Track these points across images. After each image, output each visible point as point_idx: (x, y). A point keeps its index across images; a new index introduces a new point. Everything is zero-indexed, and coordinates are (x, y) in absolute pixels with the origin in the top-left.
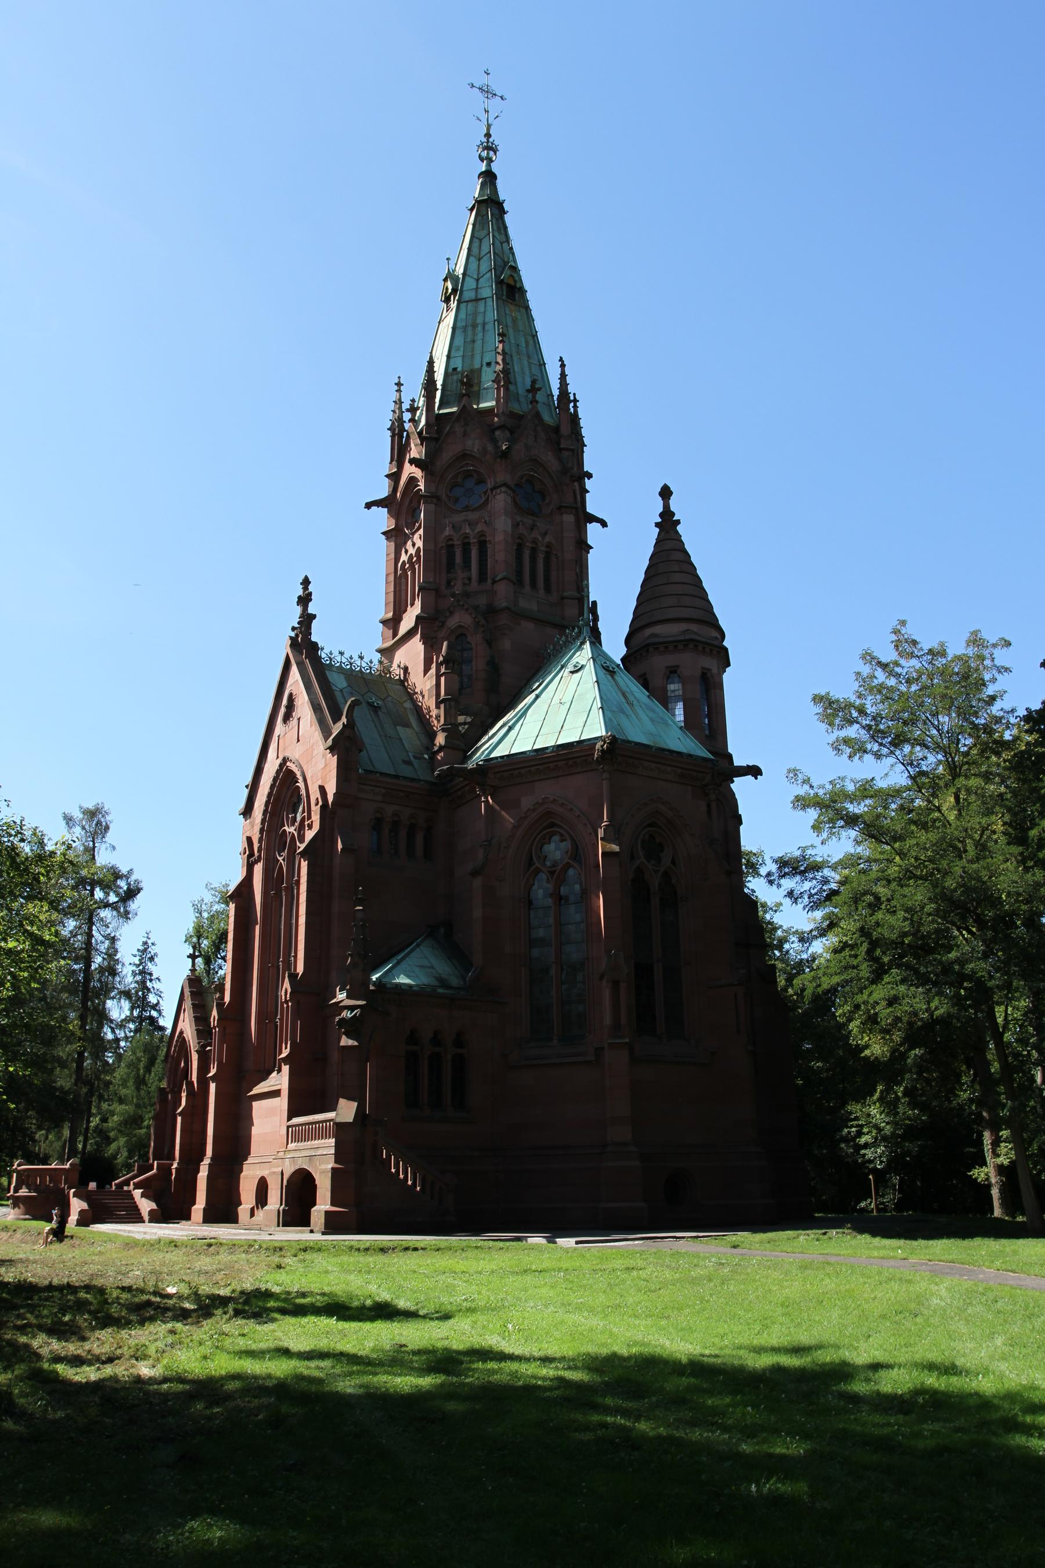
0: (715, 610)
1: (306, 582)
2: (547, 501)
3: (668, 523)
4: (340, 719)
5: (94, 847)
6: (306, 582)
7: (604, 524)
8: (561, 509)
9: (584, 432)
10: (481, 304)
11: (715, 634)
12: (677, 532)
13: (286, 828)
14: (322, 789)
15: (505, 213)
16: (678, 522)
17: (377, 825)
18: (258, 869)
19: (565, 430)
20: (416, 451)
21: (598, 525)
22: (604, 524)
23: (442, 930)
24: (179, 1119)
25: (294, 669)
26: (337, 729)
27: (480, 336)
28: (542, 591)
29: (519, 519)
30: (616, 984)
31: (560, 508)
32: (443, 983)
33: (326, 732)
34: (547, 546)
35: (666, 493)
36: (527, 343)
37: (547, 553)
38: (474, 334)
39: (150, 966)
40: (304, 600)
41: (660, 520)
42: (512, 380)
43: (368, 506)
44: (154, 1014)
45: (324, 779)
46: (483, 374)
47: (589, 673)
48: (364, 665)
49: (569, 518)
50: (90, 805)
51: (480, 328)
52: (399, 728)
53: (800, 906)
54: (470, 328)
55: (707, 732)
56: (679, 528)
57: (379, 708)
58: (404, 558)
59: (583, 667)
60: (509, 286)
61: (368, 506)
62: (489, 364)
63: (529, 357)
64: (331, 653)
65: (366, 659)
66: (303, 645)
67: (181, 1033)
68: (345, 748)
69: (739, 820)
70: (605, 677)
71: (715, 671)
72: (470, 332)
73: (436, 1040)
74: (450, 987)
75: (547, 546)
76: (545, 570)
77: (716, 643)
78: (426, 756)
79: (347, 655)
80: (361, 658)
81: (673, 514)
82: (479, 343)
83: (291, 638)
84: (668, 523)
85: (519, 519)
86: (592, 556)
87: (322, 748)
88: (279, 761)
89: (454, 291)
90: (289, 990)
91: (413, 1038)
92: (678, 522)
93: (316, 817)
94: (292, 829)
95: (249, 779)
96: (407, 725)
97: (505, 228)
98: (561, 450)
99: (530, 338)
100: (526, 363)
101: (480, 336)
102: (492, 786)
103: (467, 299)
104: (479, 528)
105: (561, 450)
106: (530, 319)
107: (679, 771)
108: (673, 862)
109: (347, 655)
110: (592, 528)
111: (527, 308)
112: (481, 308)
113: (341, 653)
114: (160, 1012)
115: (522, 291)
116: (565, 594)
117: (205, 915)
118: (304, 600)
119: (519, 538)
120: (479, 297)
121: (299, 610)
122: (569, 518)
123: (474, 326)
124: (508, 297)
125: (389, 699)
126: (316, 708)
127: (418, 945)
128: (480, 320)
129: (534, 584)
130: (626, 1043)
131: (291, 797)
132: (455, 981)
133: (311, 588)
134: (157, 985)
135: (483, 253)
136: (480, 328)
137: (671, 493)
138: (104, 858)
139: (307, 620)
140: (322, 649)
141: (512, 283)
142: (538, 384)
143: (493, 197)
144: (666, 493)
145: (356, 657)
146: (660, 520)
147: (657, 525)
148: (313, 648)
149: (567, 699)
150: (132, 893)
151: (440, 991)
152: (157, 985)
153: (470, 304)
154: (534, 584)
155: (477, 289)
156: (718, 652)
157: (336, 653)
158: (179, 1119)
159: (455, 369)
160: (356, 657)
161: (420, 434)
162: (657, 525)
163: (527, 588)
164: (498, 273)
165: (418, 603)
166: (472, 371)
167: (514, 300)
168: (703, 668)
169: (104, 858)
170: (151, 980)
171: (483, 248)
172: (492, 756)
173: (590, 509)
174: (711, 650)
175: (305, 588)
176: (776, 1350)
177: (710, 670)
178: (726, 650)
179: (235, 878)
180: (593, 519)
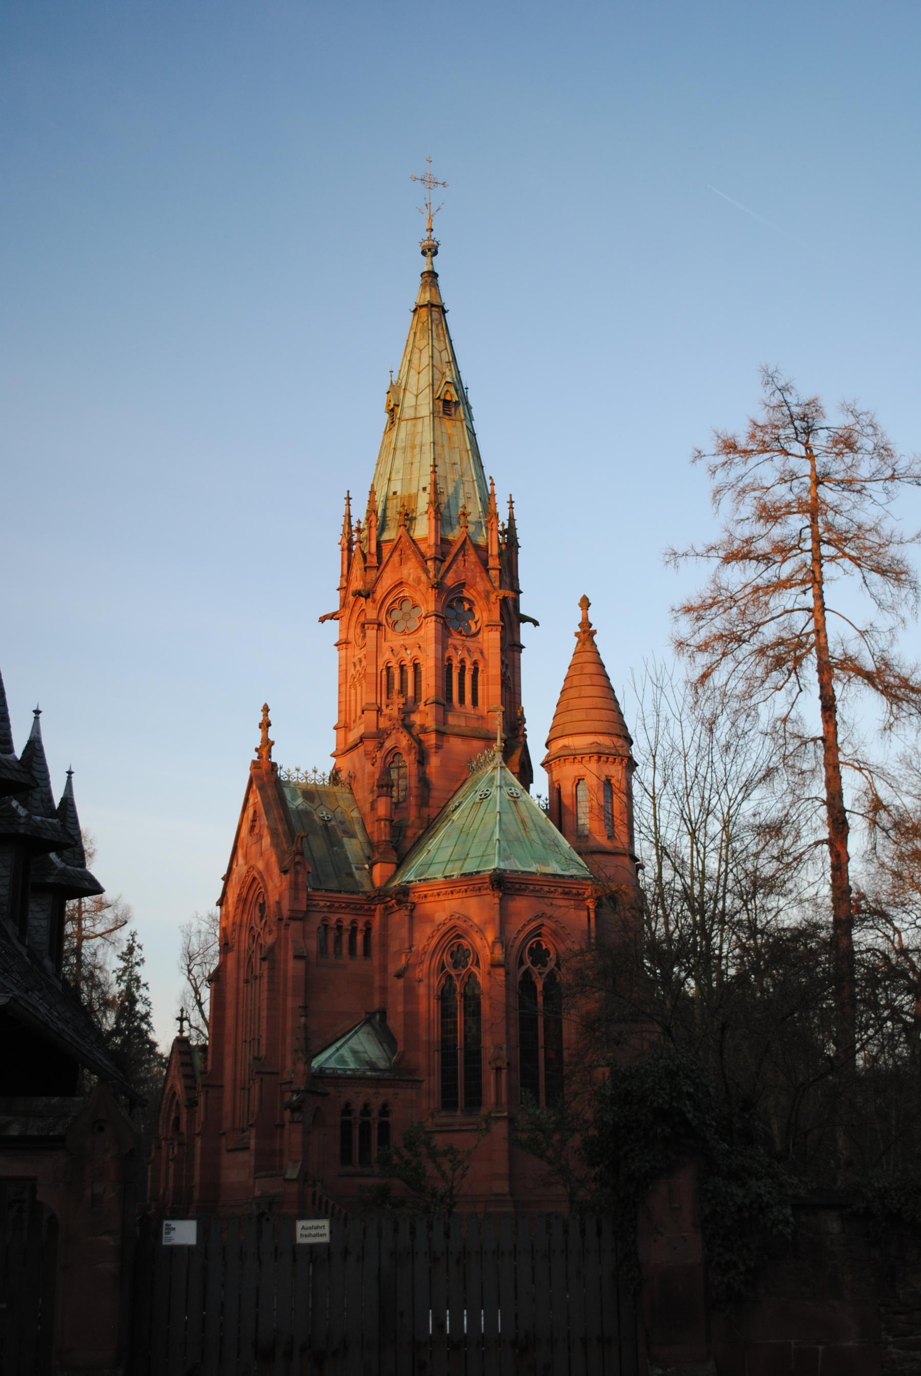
1: (266, 709)
3: (586, 633)
6: (266, 709)
7: (536, 623)
10: (420, 422)
16: (594, 632)
21: (531, 624)
22: (536, 623)
23: (378, 1017)
27: (418, 457)
30: (498, 1069)
32: (372, 1066)
35: (585, 603)
38: (413, 456)
39: (138, 971)
40: (266, 725)
41: (579, 630)
43: (322, 620)
44: (144, 1026)
46: (419, 500)
48: (318, 778)
51: (417, 450)
53: (389, 1119)
54: (409, 449)
61: (322, 620)
62: (424, 489)
64: (289, 771)
67: (172, 1087)
72: (409, 454)
73: (366, 1110)
74: (378, 1070)
79: (302, 771)
80: (315, 772)
82: (416, 465)
84: (586, 633)
86: (524, 656)
91: (347, 1110)
101: (418, 457)
103: (407, 417)
109: (302, 771)
110: (525, 628)
112: (419, 429)
113: (298, 770)
114: (149, 1024)
118: (266, 725)
120: (418, 416)
121: (259, 733)
123: (413, 447)
124: (445, 413)
127: (356, 1032)
128: (418, 442)
130: (505, 1117)
131: (257, 898)
132: (382, 1064)
135: (422, 366)
136: (417, 450)
137: (589, 604)
139: (267, 745)
144: (585, 603)
145: (310, 772)
146: (579, 630)
147: (577, 634)
151: (369, 1073)
152: (143, 991)
153: (410, 423)
155: (416, 406)
157: (293, 770)
159: (395, 493)
160: (310, 772)
162: (577, 634)
166: (410, 496)
168: (606, 776)
170: (138, 988)
171: (423, 360)
173: (523, 611)
175: (266, 715)
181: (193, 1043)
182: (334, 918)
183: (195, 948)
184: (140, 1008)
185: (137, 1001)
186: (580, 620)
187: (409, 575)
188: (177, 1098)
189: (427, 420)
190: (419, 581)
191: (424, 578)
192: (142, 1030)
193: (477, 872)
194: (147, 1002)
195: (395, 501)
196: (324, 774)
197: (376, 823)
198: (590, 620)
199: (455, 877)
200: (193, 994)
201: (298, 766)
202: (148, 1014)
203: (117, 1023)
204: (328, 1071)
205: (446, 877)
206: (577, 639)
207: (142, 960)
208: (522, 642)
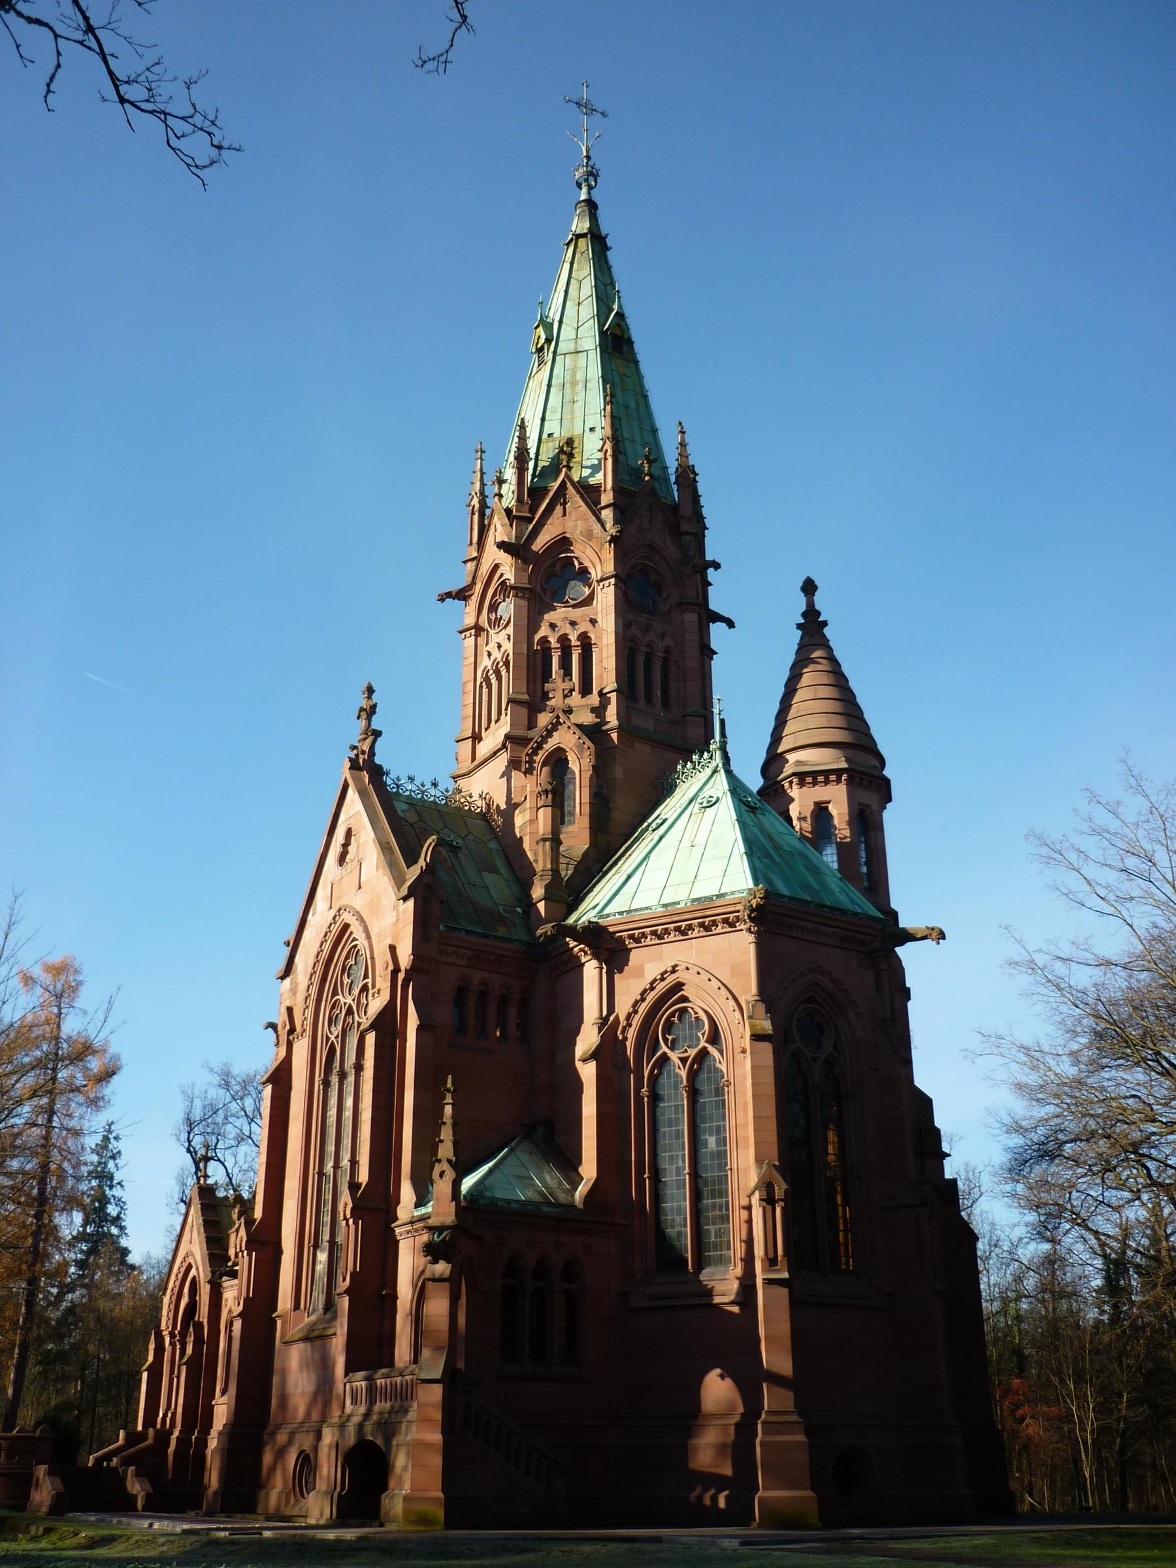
0: (872, 731)
2: (664, 595)
4: (416, 861)
5: (60, 1013)
7: (730, 624)
8: (682, 605)
9: (705, 512)
11: (875, 762)
12: (824, 636)
13: (340, 997)
14: (392, 948)
15: (608, 249)
16: (825, 623)
17: (461, 993)
18: (301, 1050)
19: (686, 511)
20: (500, 530)
22: (730, 624)
23: (541, 1131)
24: (145, 1375)
25: (352, 794)
26: (413, 873)
28: (659, 706)
29: (631, 617)
31: (680, 605)
33: (398, 881)
34: (665, 651)
35: (809, 587)
36: (637, 404)
37: (666, 661)
38: (574, 393)
42: (621, 449)
44: (114, 1231)
45: (396, 936)
47: (727, 810)
49: (691, 618)
50: (55, 958)
51: (581, 386)
52: (485, 875)
55: (866, 884)
56: (826, 630)
57: (459, 848)
58: (485, 662)
59: (718, 800)
60: (614, 336)
61: (442, 598)
62: (592, 430)
63: (640, 421)
65: (441, 787)
66: (367, 768)
68: (425, 895)
69: (906, 994)
70: (749, 817)
71: (875, 807)
75: (665, 651)
76: (645, 676)
77: (875, 773)
78: (519, 910)
79: (418, 782)
80: (435, 785)
81: (818, 614)
82: (579, 405)
83: (351, 760)
85: (631, 617)
86: (716, 664)
87: (393, 897)
88: (333, 912)
89: (548, 341)
90: (350, 1205)
92: (825, 623)
93: (384, 984)
94: (349, 1000)
95: (291, 935)
96: (494, 870)
97: (609, 268)
98: (681, 534)
99: (641, 400)
100: (636, 429)
102: (607, 950)
104: (581, 628)
105: (681, 534)
106: (639, 377)
107: (842, 933)
108: (835, 1048)
109: (418, 782)
110: (717, 631)
111: (636, 363)
113: (411, 779)
114: (122, 1228)
115: (630, 342)
116: (688, 710)
117: (198, 1103)
119: (632, 641)
120: (580, 349)
122: (691, 618)
123: (574, 383)
124: (614, 349)
125: (471, 837)
126: (385, 848)
128: (580, 376)
129: (649, 698)
133: (375, 698)
134: (117, 1192)
137: (816, 588)
138: (71, 1026)
140: (388, 774)
141: (618, 333)
142: (655, 457)
143: (595, 231)
144: (809, 587)
145: (428, 785)
147: (799, 626)
148: (377, 773)
149: (701, 839)
150: (107, 1075)
152: (117, 1192)
154: (649, 698)
156: (879, 785)
158: (145, 1375)
159: (550, 435)
160: (428, 785)
161: (508, 511)
162: (799, 626)
163: (642, 703)
164: (602, 321)
165: (506, 720)
167: (622, 353)
168: (860, 804)
169: (71, 1026)
170: (111, 1187)
172: (606, 912)
173: (713, 606)
174: (870, 782)
176: (1110, 1559)
177: (868, 806)
178: (887, 782)
179: (266, 1057)
180: (717, 618)
181: (221, 1194)
182: (477, 977)
183: (197, 1114)
184: (112, 1210)
185: (109, 1202)
186: (804, 608)
187: (576, 527)
188: (193, 1272)
189: (592, 354)
190: (589, 535)
191: (597, 528)
192: (112, 1236)
193: (720, 896)
194: (119, 1202)
195: (551, 445)
196: (447, 791)
197: (541, 844)
198: (818, 607)
199: (682, 905)
200: (194, 1170)
201: (412, 774)
202: (118, 1218)
203: (84, 1226)
204: (500, 1204)
205: (665, 906)
206: (799, 633)
207: (119, 1152)
208: (713, 646)
